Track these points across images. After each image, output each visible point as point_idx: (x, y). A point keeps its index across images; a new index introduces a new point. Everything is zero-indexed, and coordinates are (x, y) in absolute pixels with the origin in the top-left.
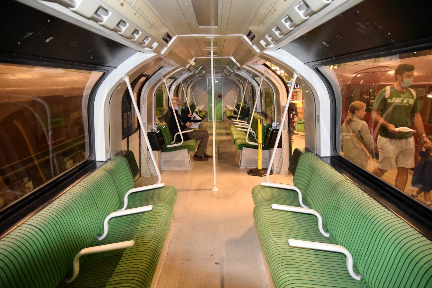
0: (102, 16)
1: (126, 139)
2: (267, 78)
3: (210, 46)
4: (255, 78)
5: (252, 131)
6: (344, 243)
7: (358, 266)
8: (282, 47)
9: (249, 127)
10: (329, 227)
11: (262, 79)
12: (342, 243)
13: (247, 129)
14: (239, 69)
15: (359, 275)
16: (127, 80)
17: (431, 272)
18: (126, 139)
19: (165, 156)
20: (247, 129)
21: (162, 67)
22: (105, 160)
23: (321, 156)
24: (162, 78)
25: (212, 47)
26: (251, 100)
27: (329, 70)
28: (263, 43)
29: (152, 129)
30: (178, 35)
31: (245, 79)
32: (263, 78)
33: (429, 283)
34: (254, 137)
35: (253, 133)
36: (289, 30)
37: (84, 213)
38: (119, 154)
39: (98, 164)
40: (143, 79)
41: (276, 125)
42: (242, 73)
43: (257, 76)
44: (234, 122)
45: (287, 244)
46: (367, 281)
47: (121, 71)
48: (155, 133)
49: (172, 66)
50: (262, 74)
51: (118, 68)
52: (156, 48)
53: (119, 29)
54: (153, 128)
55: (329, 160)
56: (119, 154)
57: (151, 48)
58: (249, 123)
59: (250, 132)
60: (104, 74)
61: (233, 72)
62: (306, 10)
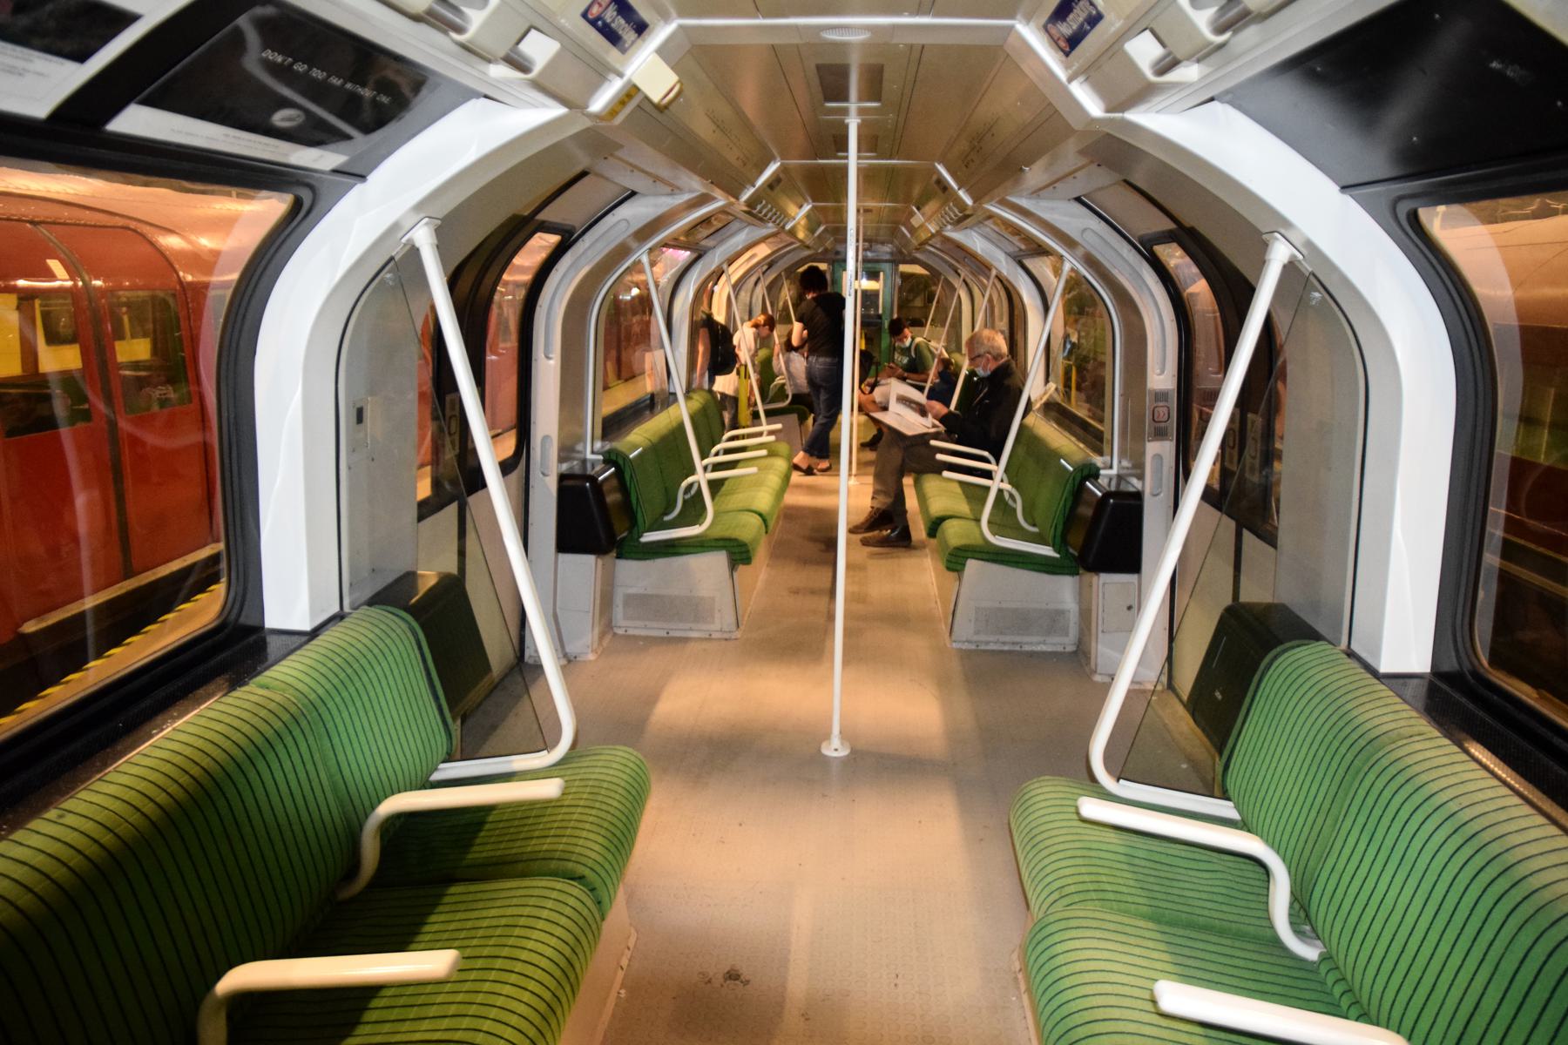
0: (464, 9)
1: (454, 507)
2: (1091, 261)
3: (846, 99)
4: (1028, 263)
5: (1006, 486)
6: (1396, 1014)
7: (1342, 956)
8: (1227, 92)
9: (999, 470)
10: (1321, 909)
11: (1067, 267)
12: (1396, 1014)
13: (988, 475)
14: (962, 219)
15: (1318, 943)
16: (424, 238)
17: (1567, 957)
18: (454, 507)
19: (634, 575)
20: (988, 475)
21: (633, 194)
22: (307, 627)
23: (1384, 669)
24: (634, 245)
25: (853, 105)
26: (1160, 434)
27: (1460, 232)
28: (1144, 51)
29: (584, 461)
30: (681, 14)
31: (982, 267)
32: (1071, 263)
33: (1542, 976)
34: (1015, 510)
35: (1011, 495)
36: (1210, 43)
37: (356, 745)
38: (394, 595)
39: (274, 644)
40: (543, 242)
41: (1114, 471)
42: (975, 241)
43: (1041, 251)
44: (940, 457)
45: (1149, 1007)
46: (1341, 964)
47: (396, 194)
48: (593, 479)
49: (675, 189)
50: (1069, 243)
51: (372, 178)
52: (542, 73)
53: (458, 20)
54: (589, 456)
55: (1417, 690)
56: (394, 595)
57: (518, 63)
58: (998, 463)
59: (1000, 491)
60: (297, 205)
61: (939, 233)
62: (1222, 8)
